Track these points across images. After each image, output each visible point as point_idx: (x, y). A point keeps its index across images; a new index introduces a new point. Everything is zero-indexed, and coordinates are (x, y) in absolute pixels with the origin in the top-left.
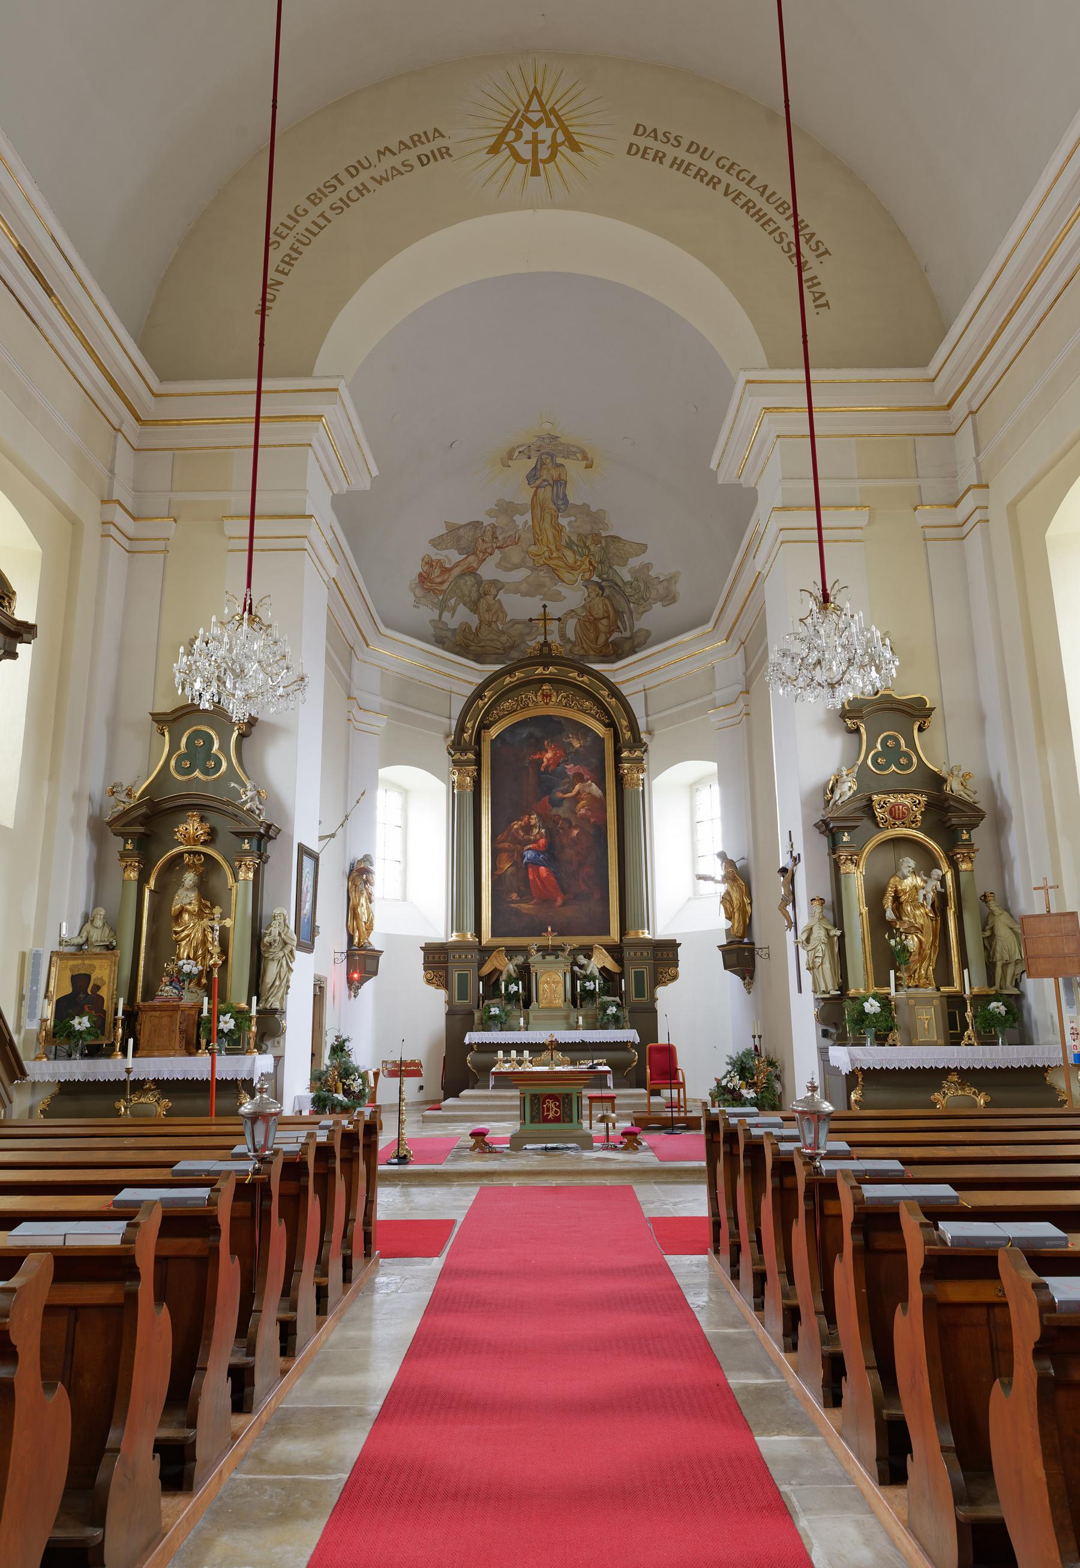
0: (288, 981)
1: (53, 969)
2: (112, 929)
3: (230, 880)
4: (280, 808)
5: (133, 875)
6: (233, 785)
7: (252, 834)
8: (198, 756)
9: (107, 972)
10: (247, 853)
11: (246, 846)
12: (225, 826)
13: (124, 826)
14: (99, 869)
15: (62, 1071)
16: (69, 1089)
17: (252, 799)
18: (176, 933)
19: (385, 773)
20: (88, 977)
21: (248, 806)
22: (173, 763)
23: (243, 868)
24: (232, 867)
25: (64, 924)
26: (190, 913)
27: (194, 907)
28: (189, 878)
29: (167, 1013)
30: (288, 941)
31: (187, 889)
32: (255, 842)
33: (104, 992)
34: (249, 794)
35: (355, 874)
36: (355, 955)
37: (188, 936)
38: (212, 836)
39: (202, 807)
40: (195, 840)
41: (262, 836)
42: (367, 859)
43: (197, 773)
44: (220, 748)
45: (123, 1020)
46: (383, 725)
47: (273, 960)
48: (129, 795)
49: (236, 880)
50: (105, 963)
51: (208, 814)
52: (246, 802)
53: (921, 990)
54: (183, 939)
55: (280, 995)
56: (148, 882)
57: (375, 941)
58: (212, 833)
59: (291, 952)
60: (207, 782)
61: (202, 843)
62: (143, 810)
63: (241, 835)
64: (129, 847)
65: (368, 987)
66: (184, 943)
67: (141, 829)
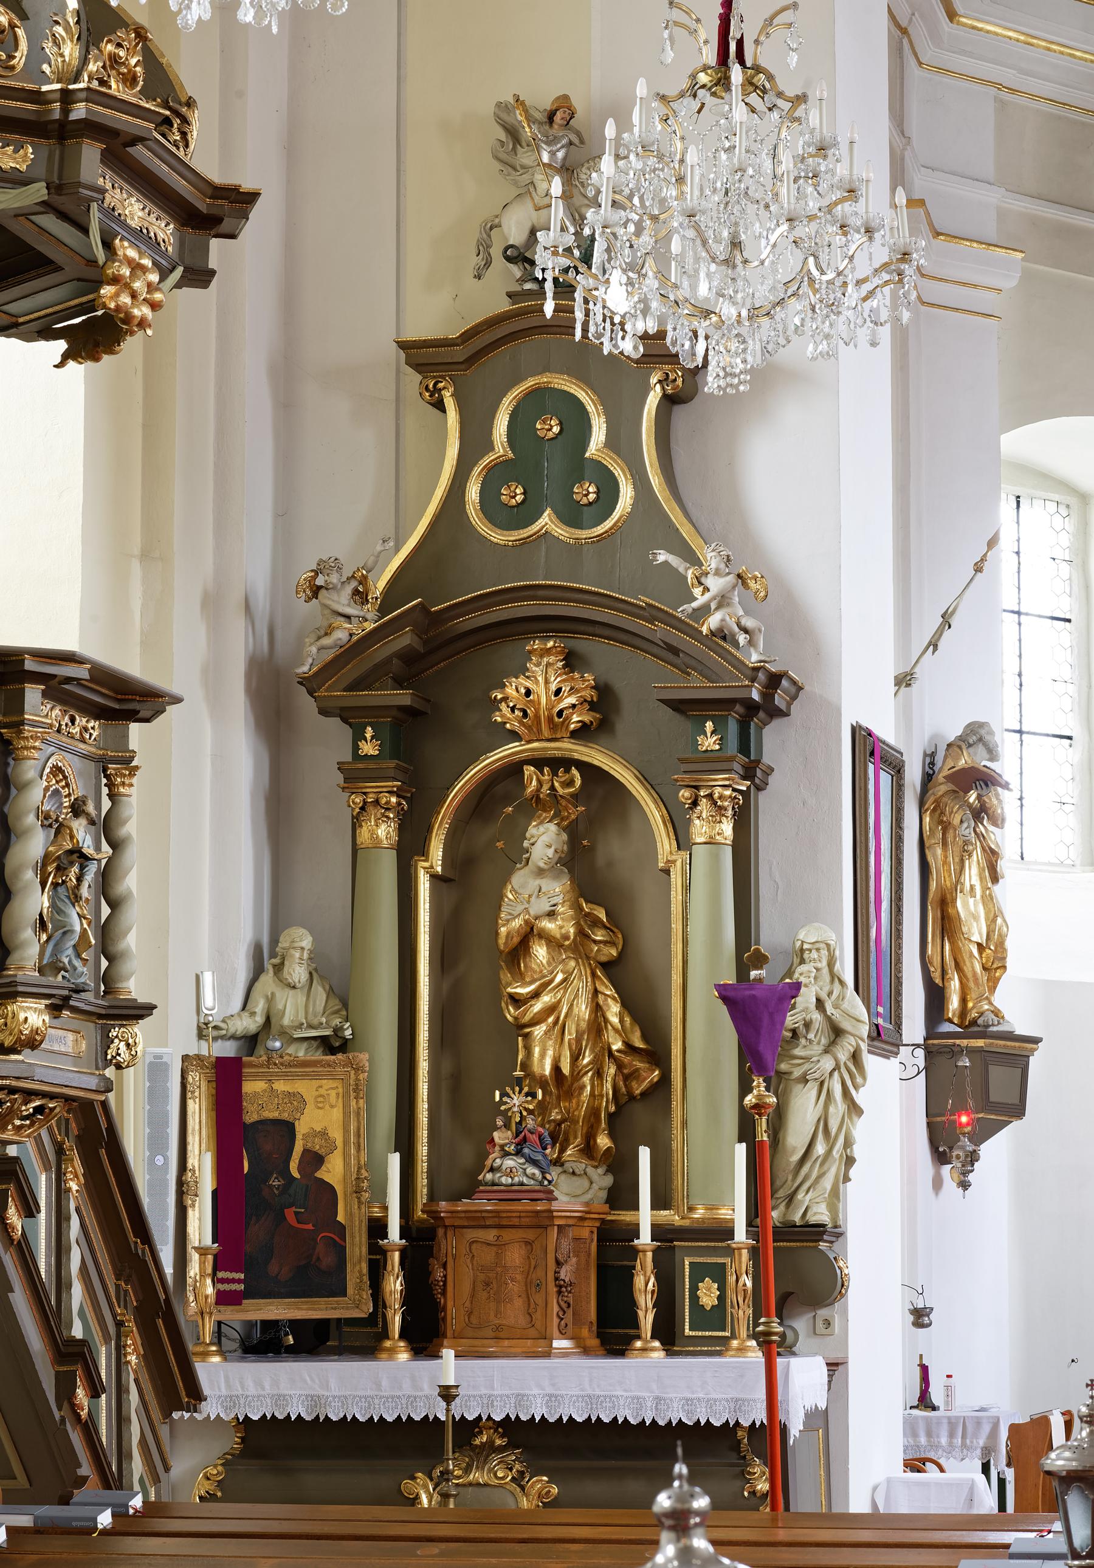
0: (848, 1143)
1: (192, 1106)
2: (331, 992)
3: (665, 844)
4: (795, 621)
5: (385, 831)
6: (662, 556)
7: (727, 704)
8: (547, 467)
9: (337, 1114)
10: (714, 762)
11: (709, 742)
12: (643, 681)
13: (354, 686)
14: (280, 811)
15: (252, 1391)
16: (271, 1447)
17: (723, 601)
18: (517, 1001)
19: (1022, 442)
20: (286, 1129)
21: (714, 621)
22: (473, 492)
23: (704, 805)
24: (665, 801)
25: (208, 979)
26: (554, 943)
27: (563, 926)
28: (544, 839)
29: (520, 1234)
30: (846, 1025)
31: (540, 872)
32: (733, 727)
33: (333, 1172)
34: (715, 584)
35: (941, 788)
36: (954, 1053)
37: (552, 1009)
38: (604, 714)
39: (570, 626)
40: (557, 721)
41: (751, 708)
42: (975, 735)
43: (547, 520)
44: (611, 443)
45: (403, 1252)
46: (1010, 282)
47: (804, 1080)
48: (360, 596)
49: (683, 841)
50: (331, 1088)
51: (584, 645)
52: (704, 611)
53: (556, 1320)
54: (535, 1022)
55: (827, 1183)
56: (423, 851)
57: (1014, 1005)
58: (604, 704)
59: (855, 1057)
60: (577, 548)
61: (575, 735)
62: (405, 639)
63: (690, 709)
64: (369, 748)
65: (997, 1152)
66: (539, 1031)
67: (403, 697)
